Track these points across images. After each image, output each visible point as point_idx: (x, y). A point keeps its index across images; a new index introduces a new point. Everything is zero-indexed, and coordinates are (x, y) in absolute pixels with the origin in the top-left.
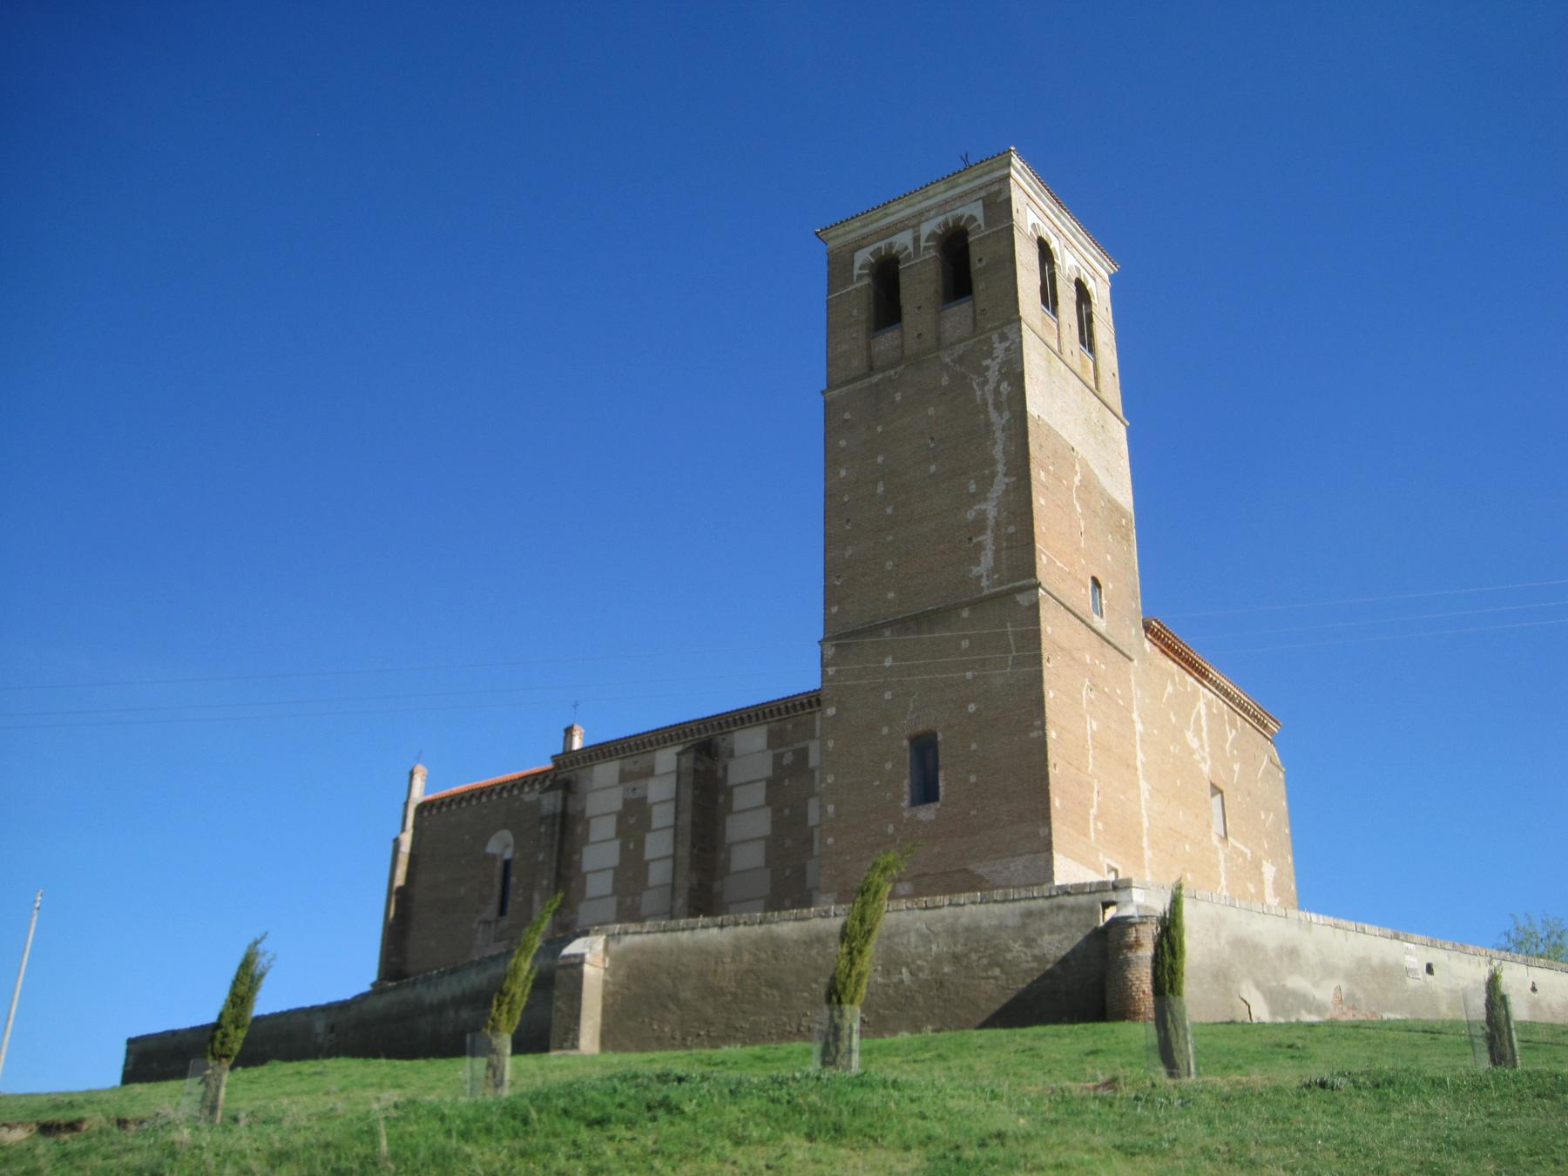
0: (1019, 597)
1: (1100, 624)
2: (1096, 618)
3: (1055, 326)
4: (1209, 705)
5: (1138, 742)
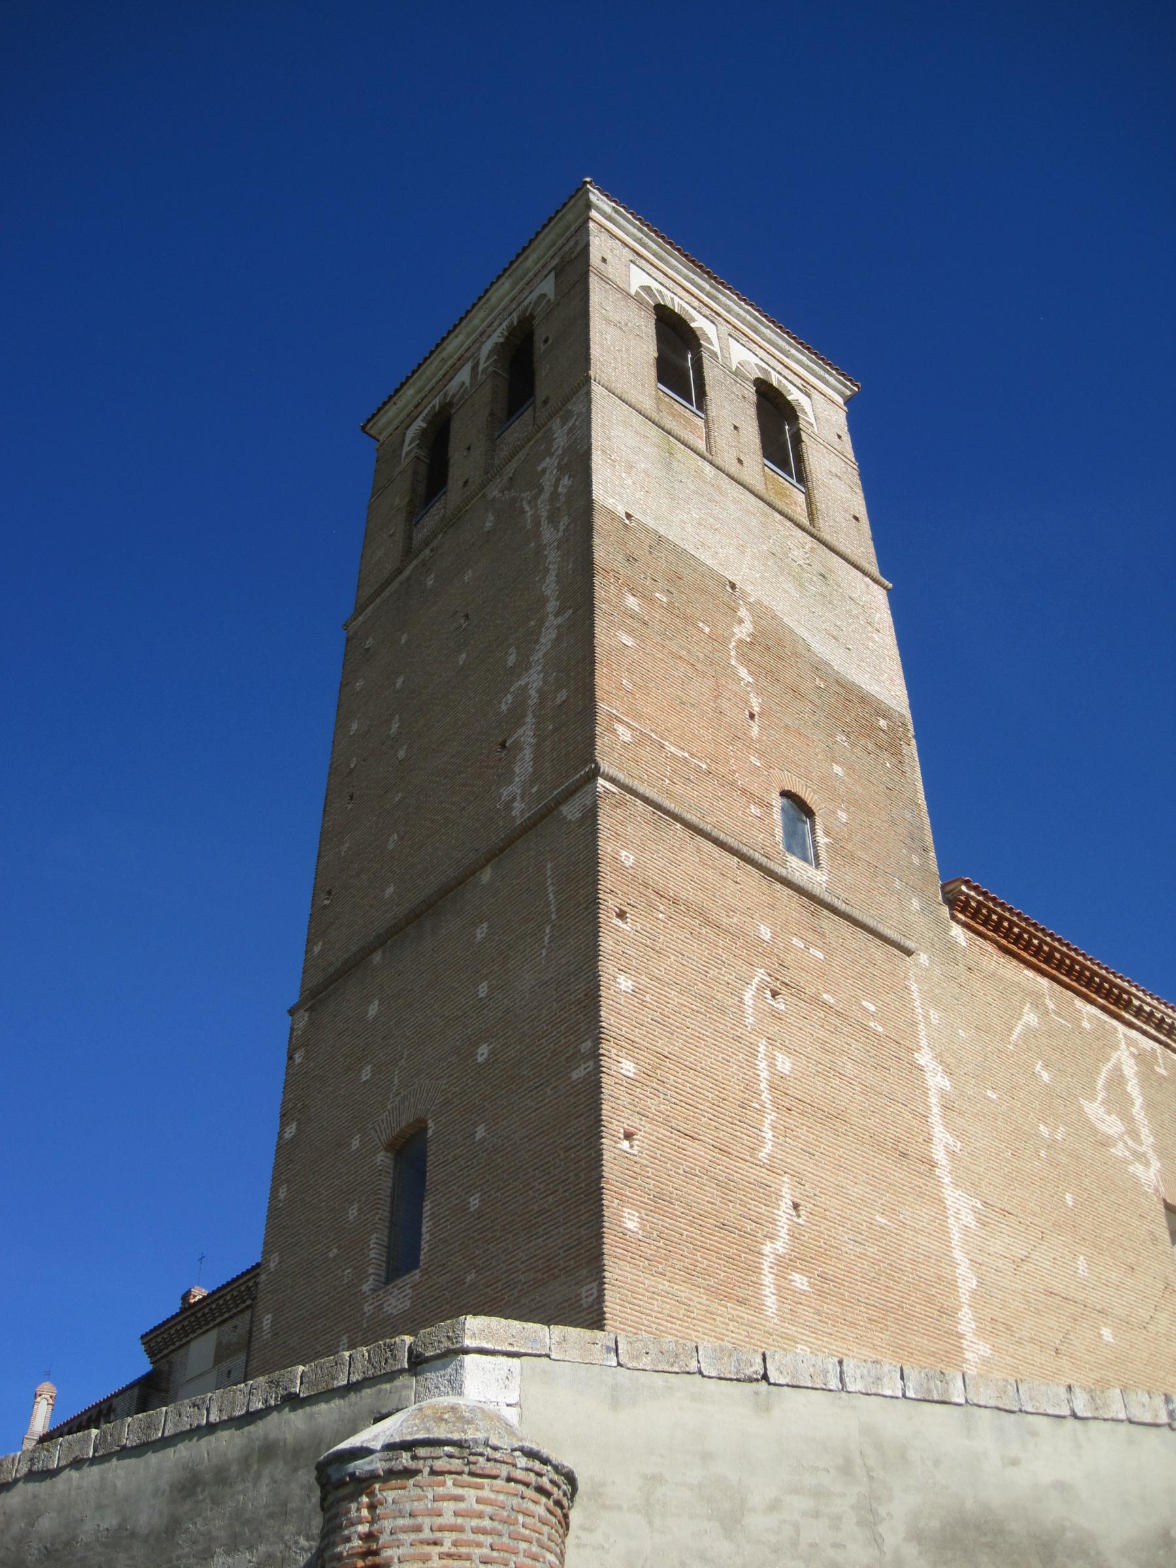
0: (565, 809)
1: (815, 878)
2: (794, 862)
3: (701, 423)
4: (1142, 1058)
5: (935, 1110)
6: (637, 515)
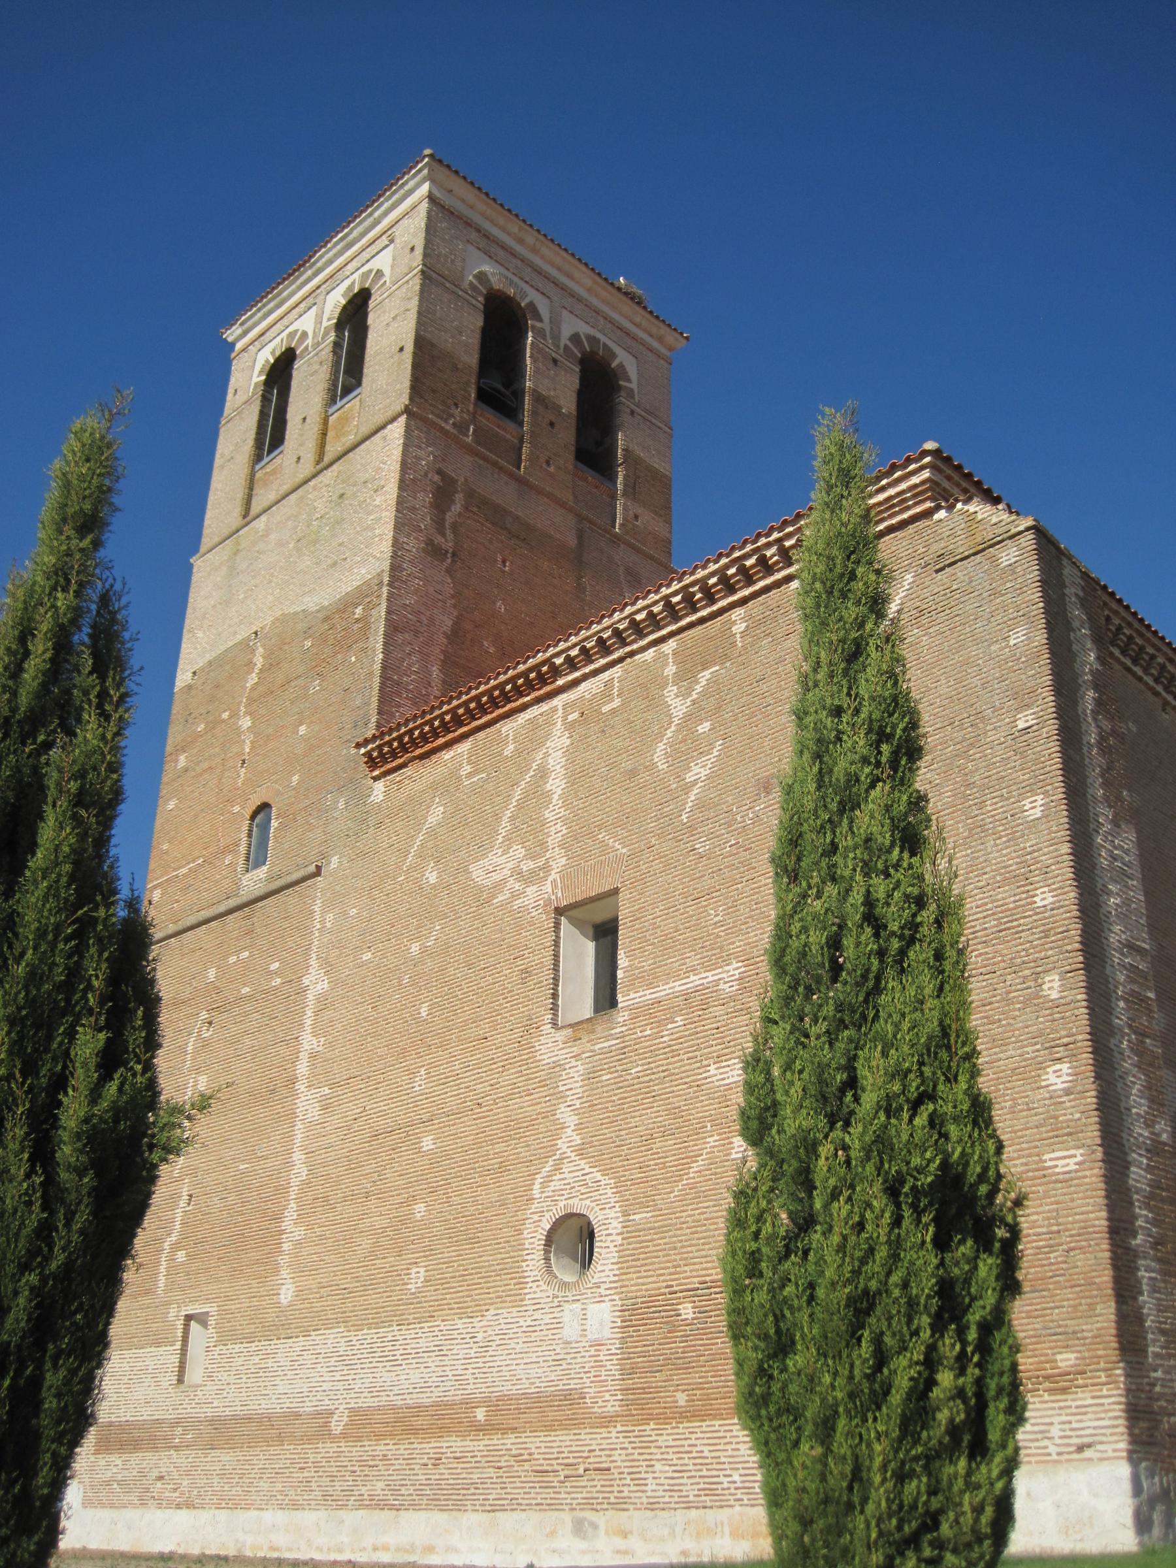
6: (196, 667)
